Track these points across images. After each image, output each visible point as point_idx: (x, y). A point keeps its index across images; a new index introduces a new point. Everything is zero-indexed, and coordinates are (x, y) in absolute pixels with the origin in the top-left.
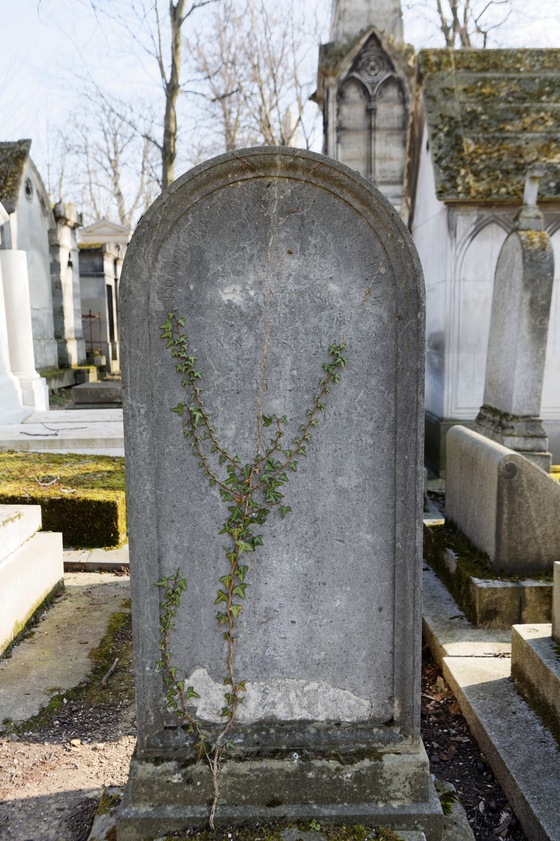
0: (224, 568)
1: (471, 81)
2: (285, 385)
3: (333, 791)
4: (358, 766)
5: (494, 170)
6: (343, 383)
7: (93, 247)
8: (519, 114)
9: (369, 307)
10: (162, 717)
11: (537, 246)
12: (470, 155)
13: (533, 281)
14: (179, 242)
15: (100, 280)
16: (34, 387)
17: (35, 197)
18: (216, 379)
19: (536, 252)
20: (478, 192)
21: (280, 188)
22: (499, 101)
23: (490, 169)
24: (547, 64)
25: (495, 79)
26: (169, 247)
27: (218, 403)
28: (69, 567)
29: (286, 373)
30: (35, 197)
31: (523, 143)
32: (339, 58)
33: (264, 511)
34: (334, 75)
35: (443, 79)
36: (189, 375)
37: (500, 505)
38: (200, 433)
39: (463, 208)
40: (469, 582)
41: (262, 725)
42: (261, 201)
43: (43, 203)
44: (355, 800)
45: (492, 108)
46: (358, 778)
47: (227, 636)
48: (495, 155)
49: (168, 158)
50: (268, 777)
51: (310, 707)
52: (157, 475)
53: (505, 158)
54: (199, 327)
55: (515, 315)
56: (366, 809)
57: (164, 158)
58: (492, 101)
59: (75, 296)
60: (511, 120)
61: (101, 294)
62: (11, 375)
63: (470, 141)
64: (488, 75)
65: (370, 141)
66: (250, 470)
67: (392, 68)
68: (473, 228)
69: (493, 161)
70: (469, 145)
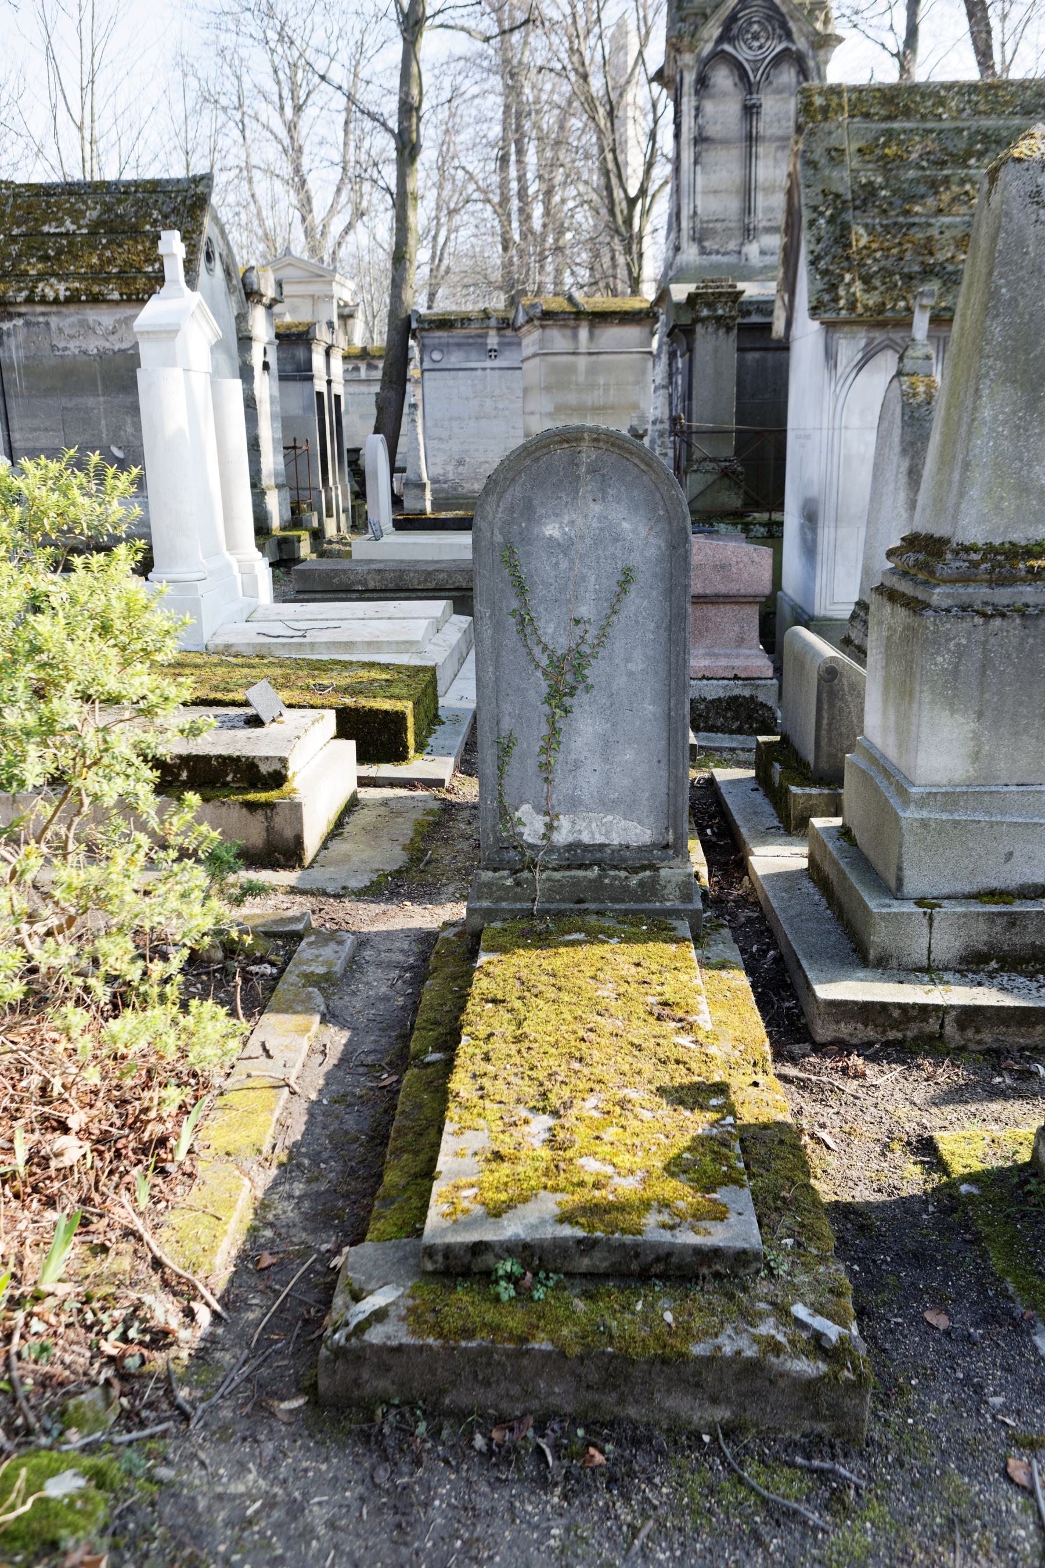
0: (545, 729)
1: (870, 136)
2: (590, 596)
3: (623, 893)
4: (641, 875)
5: (891, 274)
6: (632, 595)
7: (294, 330)
8: (934, 186)
9: (651, 539)
10: (499, 840)
11: (921, 398)
12: (859, 252)
13: (912, 444)
14: (515, 492)
15: (307, 384)
16: (257, 571)
17: (218, 266)
18: (541, 591)
19: (919, 406)
20: (866, 308)
21: (587, 454)
22: (909, 166)
23: (886, 273)
24: (982, 107)
25: (905, 132)
26: (508, 496)
27: (541, 609)
28: (364, 782)
29: (591, 587)
30: (218, 266)
31: (935, 232)
32: (699, 20)
33: (574, 688)
34: (691, 49)
35: (830, 133)
36: (521, 588)
37: (819, 710)
38: (528, 630)
39: (846, 329)
40: (787, 790)
41: (571, 847)
42: (574, 463)
43: (228, 273)
44: (638, 901)
45: (896, 178)
46: (641, 884)
47: (546, 780)
48: (895, 251)
49: (407, 152)
50: (576, 882)
51: (607, 834)
52: (497, 661)
53: (908, 256)
54: (529, 554)
55: (891, 487)
56: (646, 906)
57: (400, 150)
58: (898, 168)
59: (273, 417)
60: (923, 197)
61: (307, 408)
62: (227, 554)
63: (862, 231)
64: (896, 125)
65: (749, 159)
66: (564, 657)
67: (789, 35)
68: (860, 356)
69: (891, 260)
70: (860, 237)
